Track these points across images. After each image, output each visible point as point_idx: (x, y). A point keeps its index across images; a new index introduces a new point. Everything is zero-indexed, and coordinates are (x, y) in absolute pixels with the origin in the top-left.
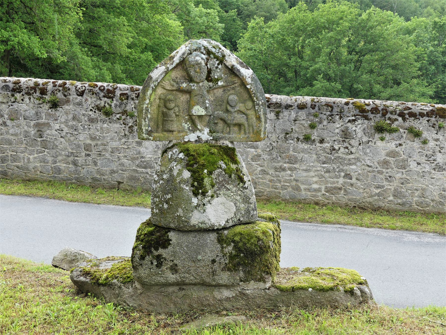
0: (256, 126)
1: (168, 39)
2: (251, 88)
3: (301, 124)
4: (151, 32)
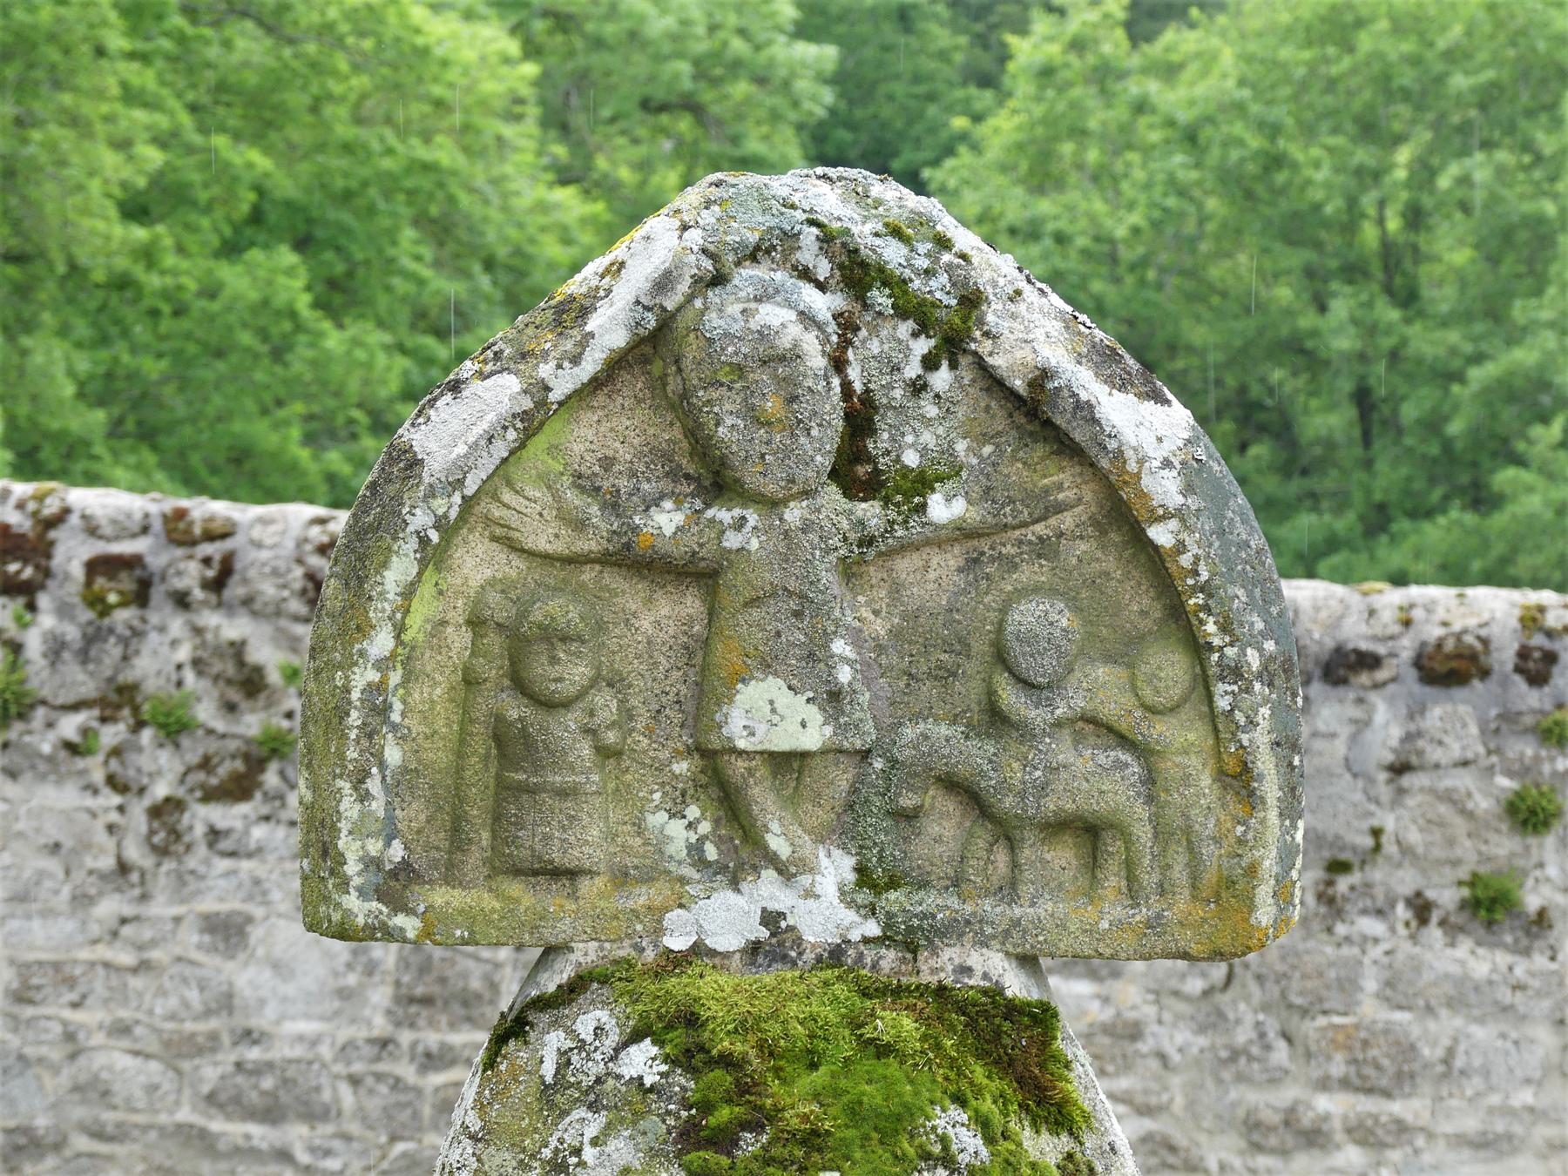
0: (1217, 841)
1: (422, 153)
2: (1180, 548)
3: (1448, 797)
4: (297, 99)
